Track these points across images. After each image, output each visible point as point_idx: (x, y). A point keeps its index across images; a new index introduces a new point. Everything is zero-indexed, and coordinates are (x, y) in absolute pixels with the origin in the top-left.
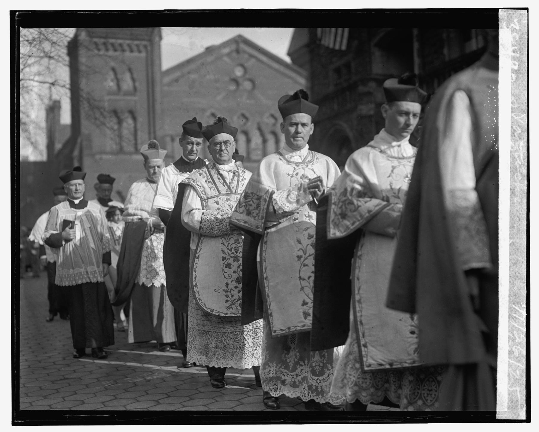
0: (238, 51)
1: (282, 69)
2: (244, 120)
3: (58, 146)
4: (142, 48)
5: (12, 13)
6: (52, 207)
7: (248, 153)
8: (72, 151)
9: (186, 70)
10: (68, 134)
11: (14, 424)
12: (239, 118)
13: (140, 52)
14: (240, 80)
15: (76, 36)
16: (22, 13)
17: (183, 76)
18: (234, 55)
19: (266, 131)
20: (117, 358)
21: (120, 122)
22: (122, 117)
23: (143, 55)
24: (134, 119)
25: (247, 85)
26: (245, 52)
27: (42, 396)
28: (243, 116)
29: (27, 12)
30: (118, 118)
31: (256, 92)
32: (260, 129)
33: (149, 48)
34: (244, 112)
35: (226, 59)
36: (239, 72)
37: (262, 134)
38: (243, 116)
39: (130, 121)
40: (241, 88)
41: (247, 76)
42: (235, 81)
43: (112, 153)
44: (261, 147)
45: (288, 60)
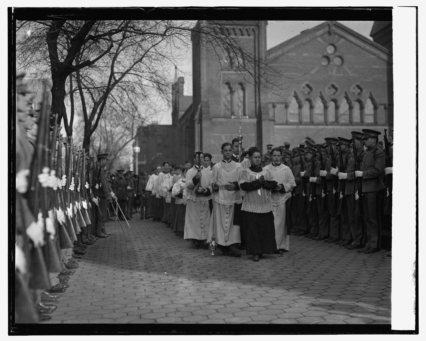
0: (329, 33)
1: (368, 47)
2: (334, 90)
3: (181, 113)
4: (251, 32)
5: (10, 9)
6: (388, 167)
7: (337, 118)
8: (193, 115)
9: (286, 49)
10: (190, 102)
11: (10, 334)
12: (329, 88)
13: (249, 35)
14: (331, 57)
15: (198, 25)
16: (310, 9)
17: (283, 54)
18: (326, 35)
19: (352, 99)
20: (245, 293)
21: (232, 92)
22: (234, 89)
23: (252, 37)
24: (243, 89)
25: (337, 61)
26: (336, 34)
27: (104, 318)
28: (358, 87)
29: (238, 9)
30: (230, 88)
31: (345, 67)
32: (347, 98)
33: (257, 32)
34: (334, 83)
35: (319, 39)
36: (330, 50)
37: (349, 103)
38: (333, 86)
39: (241, 93)
40: (331, 63)
41: (337, 54)
42: (327, 58)
43: (225, 117)
44: (348, 113)
45: (371, 39)
